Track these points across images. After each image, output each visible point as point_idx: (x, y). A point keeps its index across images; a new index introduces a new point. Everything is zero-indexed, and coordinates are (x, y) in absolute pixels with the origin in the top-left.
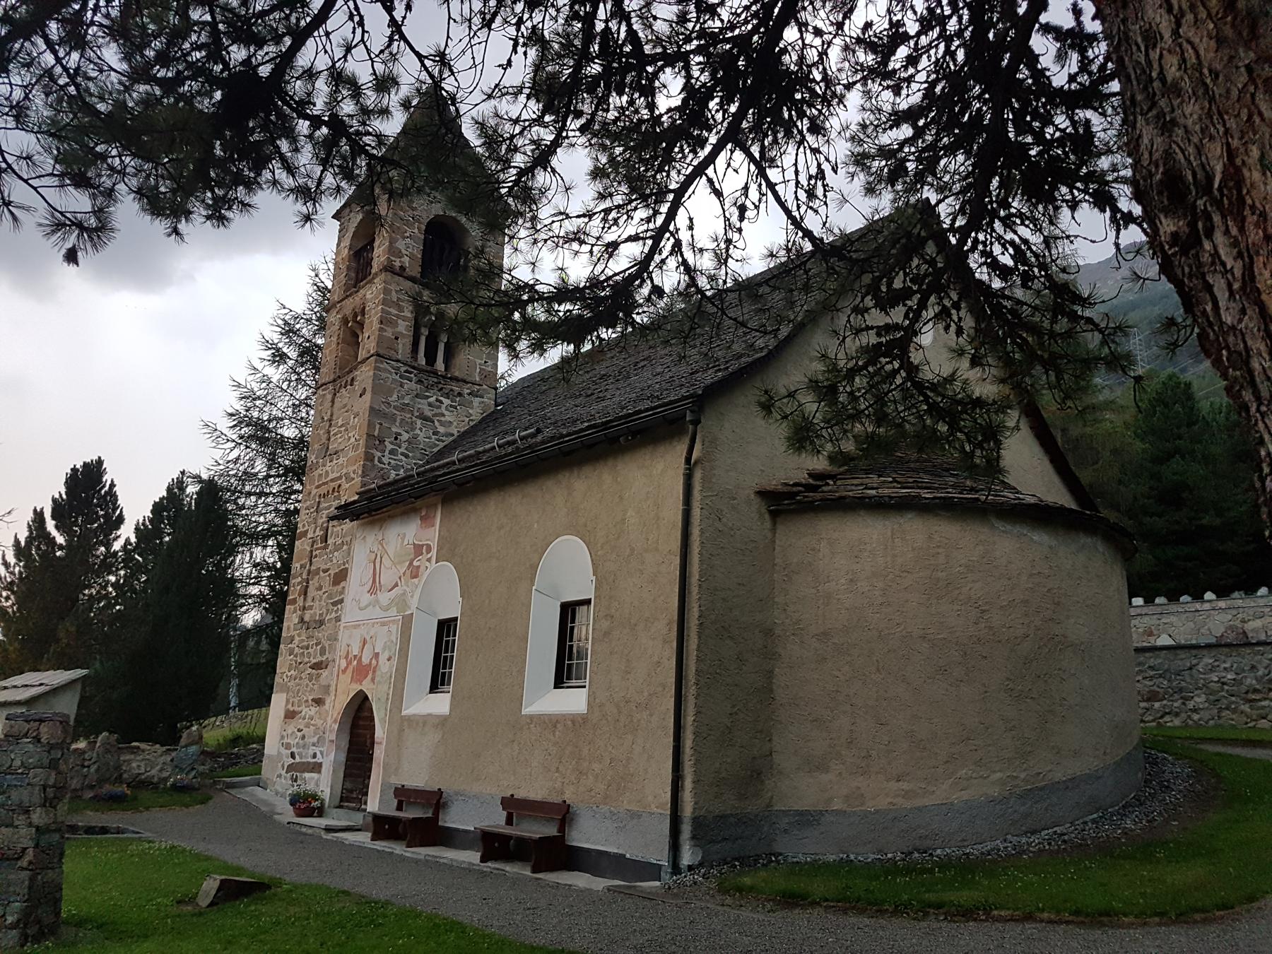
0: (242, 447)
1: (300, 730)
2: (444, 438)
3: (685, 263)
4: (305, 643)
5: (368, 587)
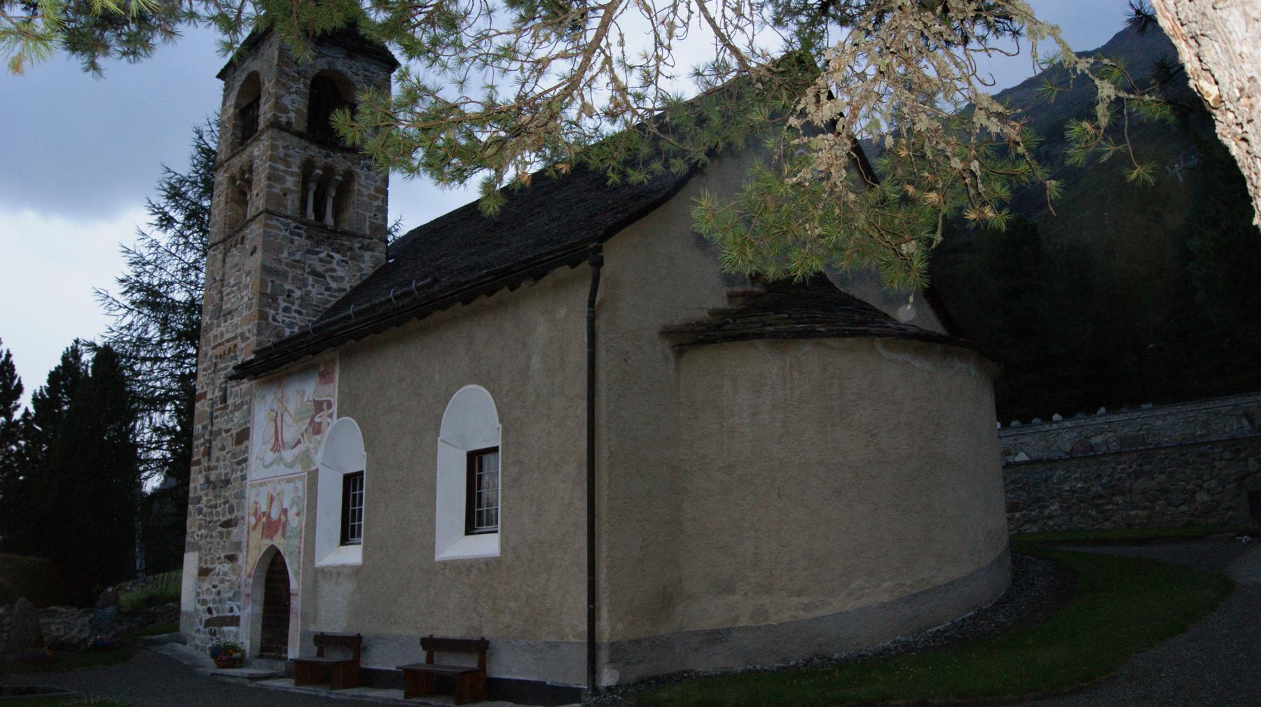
0: (135, 313)
1: (215, 587)
2: (336, 294)
3: (614, 79)
4: (213, 503)
5: (270, 446)
